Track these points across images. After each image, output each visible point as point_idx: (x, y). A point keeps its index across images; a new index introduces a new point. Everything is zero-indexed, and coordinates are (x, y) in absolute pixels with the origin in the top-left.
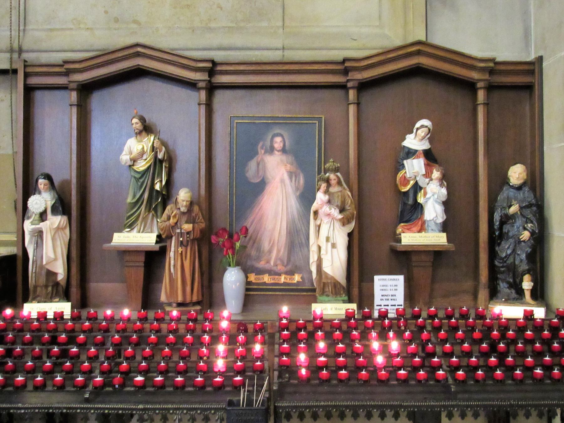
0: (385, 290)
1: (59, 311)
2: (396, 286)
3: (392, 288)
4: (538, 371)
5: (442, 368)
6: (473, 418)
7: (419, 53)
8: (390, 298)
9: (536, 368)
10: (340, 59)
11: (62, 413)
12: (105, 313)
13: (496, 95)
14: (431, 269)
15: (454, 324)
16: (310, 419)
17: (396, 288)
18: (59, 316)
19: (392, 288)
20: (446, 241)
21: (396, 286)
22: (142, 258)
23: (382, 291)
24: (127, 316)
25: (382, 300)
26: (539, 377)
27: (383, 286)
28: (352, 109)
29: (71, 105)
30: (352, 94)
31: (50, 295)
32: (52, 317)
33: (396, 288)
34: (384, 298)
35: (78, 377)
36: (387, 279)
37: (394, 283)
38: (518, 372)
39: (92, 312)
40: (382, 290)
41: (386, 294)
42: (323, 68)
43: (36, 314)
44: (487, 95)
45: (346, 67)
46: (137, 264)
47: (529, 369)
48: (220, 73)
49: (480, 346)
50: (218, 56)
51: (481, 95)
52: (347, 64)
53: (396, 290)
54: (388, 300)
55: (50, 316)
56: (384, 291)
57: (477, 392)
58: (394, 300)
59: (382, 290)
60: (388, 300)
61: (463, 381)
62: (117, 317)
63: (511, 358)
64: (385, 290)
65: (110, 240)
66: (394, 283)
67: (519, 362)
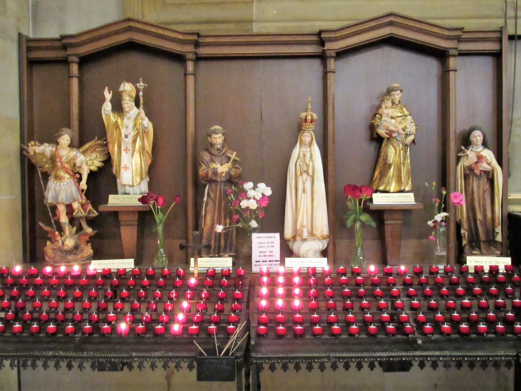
0: (262, 247)
1: (494, 264)
2: (273, 243)
3: (269, 245)
4: (500, 326)
5: (409, 323)
6: (294, 371)
7: (130, 29)
8: (268, 253)
9: (516, 323)
10: (317, 30)
11: (401, 360)
12: (399, 268)
13: (203, 65)
14: (136, 228)
15: (455, 280)
16: (330, 369)
17: (272, 245)
18: (494, 270)
19: (269, 245)
20: (413, 200)
21: (273, 243)
22: (136, 217)
23: (260, 248)
24: (404, 271)
25: (260, 256)
26: (500, 331)
27: (261, 243)
28: (75, 83)
29: (334, 72)
30: (75, 68)
31: (216, 250)
32: (488, 272)
33: (272, 245)
34: (262, 254)
35: (87, 325)
36: (264, 237)
37: (271, 240)
38: (428, 326)
39: (434, 267)
40: (260, 247)
41: (264, 251)
42: (244, 40)
43: (489, 267)
44: (195, 67)
45: (63, 44)
46: (131, 223)
47: (382, 323)
48: (447, 38)
49: (361, 302)
50: (203, 29)
51: (190, 66)
52: (64, 41)
53: (273, 246)
54: (265, 256)
55: (487, 270)
56: (262, 248)
57: (49, 342)
58: (271, 256)
59: (260, 247)
60: (265, 256)
61: (502, 335)
62: (395, 272)
63: (475, 313)
64: (262, 247)
65: (107, 202)
66: (271, 240)
67: (482, 315)
